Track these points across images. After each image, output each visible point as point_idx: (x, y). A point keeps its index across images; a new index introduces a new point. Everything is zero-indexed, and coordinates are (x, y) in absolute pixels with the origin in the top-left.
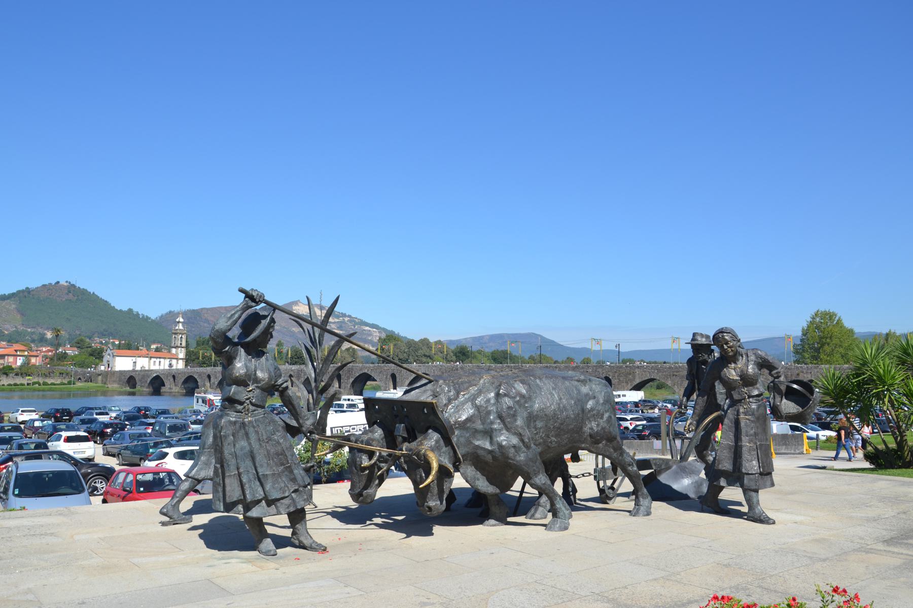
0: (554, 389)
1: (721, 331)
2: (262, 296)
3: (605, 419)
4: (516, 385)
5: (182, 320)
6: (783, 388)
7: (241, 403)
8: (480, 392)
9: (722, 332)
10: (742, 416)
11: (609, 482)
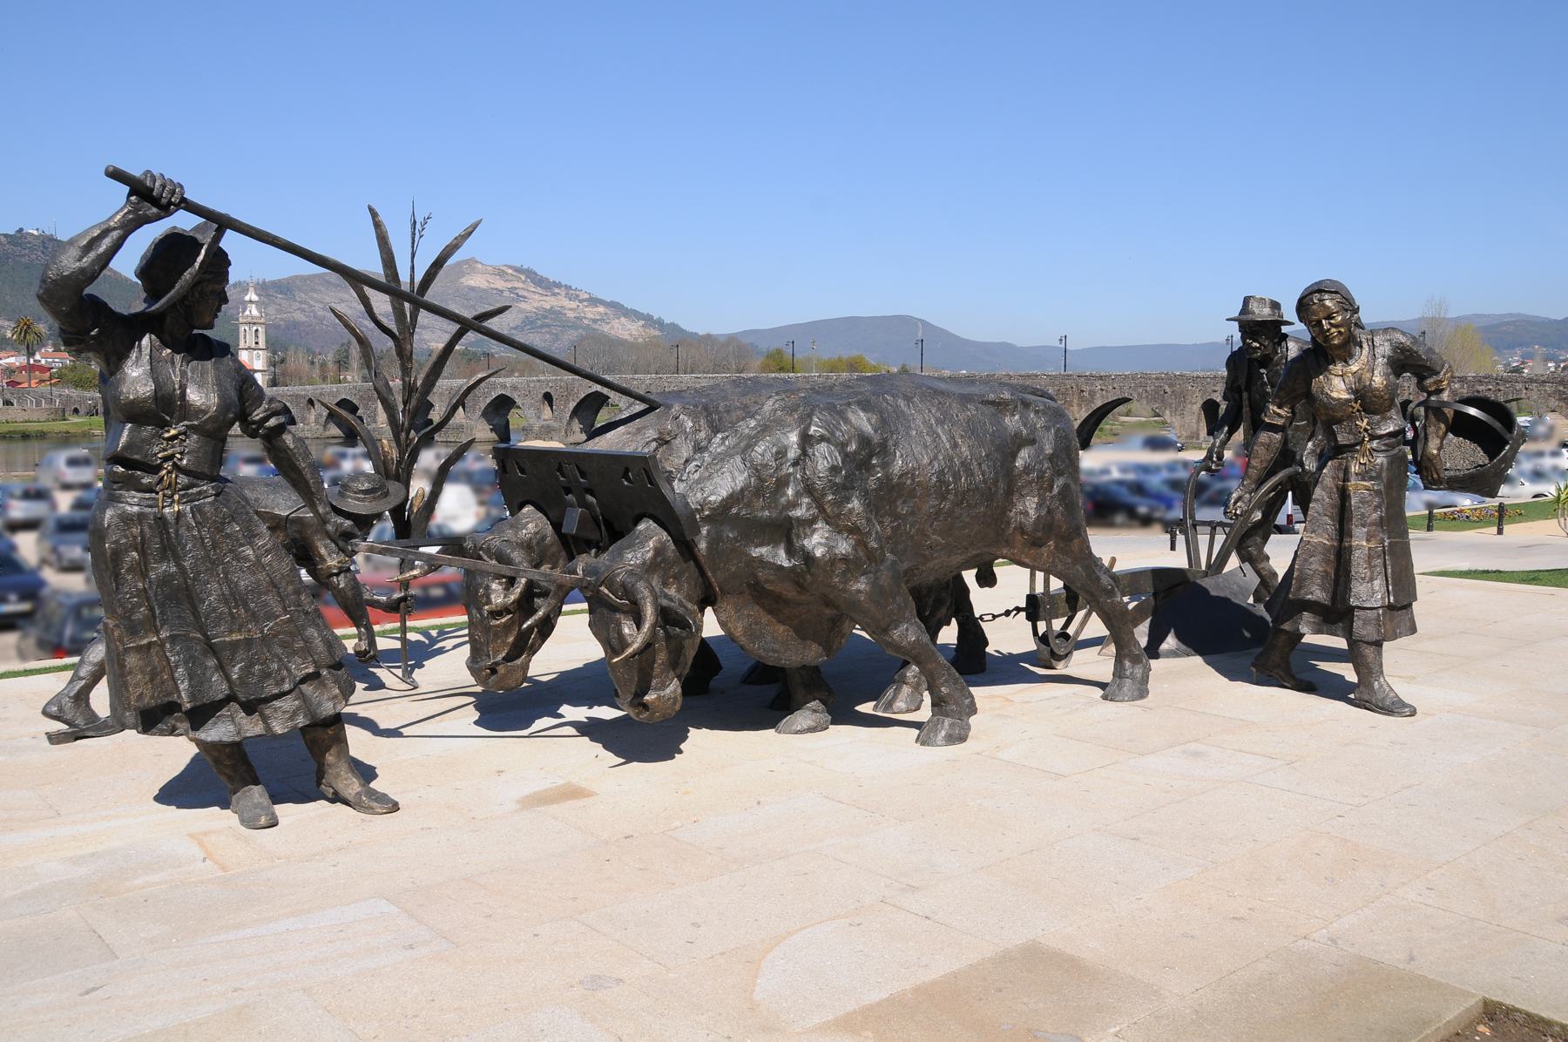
0: (939, 422)
1: (1319, 289)
2: (176, 188)
3: (1056, 490)
4: (850, 415)
5: (255, 298)
6: (1449, 413)
7: (155, 470)
8: (765, 429)
9: (1320, 291)
10: (1353, 482)
11: (1057, 624)
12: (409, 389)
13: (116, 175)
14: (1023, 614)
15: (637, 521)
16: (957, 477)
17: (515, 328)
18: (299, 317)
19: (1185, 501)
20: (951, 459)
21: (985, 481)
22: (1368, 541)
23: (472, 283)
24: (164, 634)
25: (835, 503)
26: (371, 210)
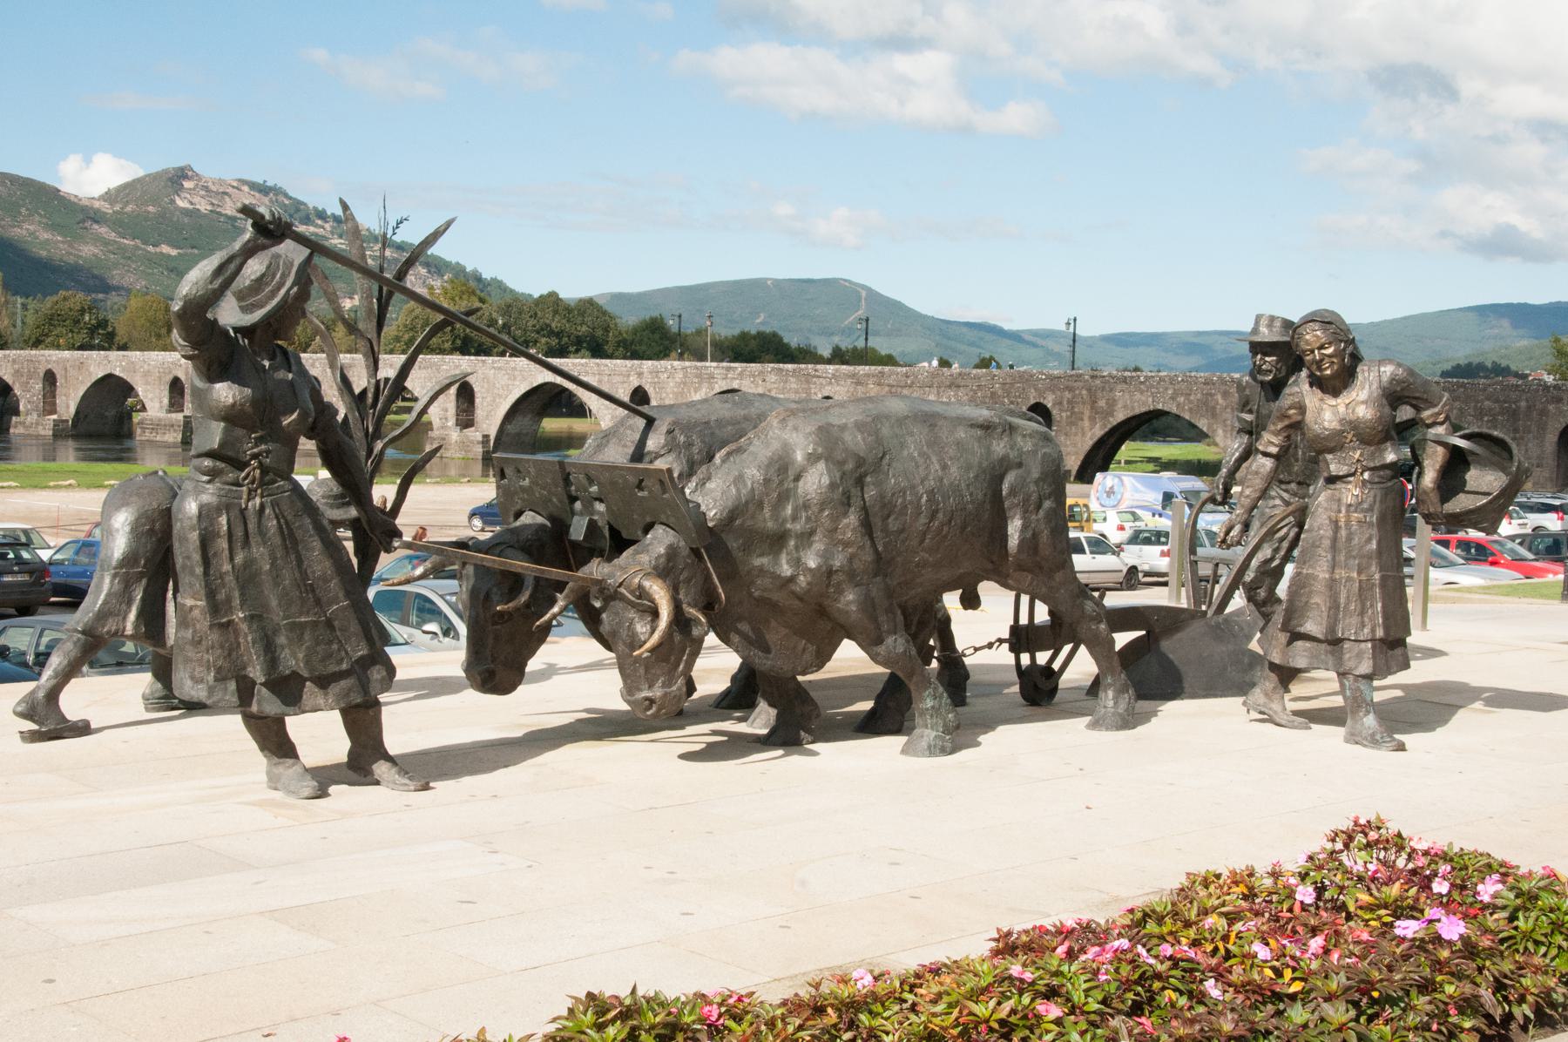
14: (1006, 646)
15: (648, 528)
16: (946, 497)
19: (479, 546)
20: (941, 480)
21: (972, 502)
26: (448, 224)
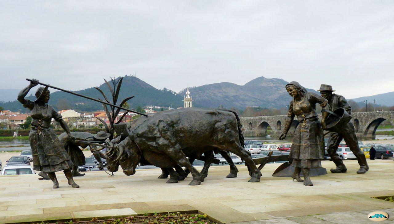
5: (189, 93)
12: (113, 115)
13: (27, 80)
17: (276, 100)
18: (206, 98)
22: (305, 144)
23: (262, 85)
24: (38, 153)
25: (163, 134)
